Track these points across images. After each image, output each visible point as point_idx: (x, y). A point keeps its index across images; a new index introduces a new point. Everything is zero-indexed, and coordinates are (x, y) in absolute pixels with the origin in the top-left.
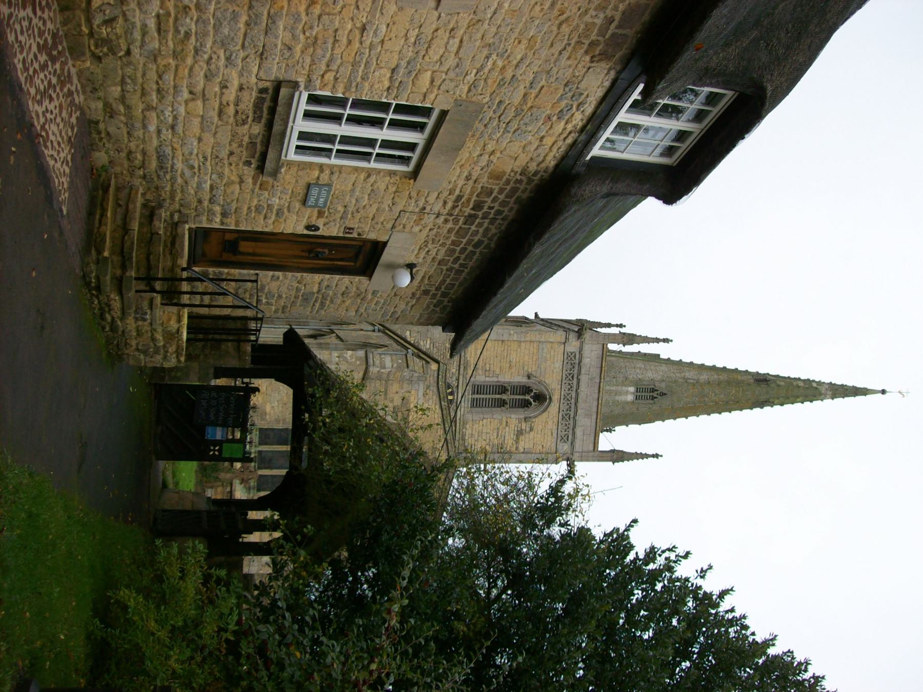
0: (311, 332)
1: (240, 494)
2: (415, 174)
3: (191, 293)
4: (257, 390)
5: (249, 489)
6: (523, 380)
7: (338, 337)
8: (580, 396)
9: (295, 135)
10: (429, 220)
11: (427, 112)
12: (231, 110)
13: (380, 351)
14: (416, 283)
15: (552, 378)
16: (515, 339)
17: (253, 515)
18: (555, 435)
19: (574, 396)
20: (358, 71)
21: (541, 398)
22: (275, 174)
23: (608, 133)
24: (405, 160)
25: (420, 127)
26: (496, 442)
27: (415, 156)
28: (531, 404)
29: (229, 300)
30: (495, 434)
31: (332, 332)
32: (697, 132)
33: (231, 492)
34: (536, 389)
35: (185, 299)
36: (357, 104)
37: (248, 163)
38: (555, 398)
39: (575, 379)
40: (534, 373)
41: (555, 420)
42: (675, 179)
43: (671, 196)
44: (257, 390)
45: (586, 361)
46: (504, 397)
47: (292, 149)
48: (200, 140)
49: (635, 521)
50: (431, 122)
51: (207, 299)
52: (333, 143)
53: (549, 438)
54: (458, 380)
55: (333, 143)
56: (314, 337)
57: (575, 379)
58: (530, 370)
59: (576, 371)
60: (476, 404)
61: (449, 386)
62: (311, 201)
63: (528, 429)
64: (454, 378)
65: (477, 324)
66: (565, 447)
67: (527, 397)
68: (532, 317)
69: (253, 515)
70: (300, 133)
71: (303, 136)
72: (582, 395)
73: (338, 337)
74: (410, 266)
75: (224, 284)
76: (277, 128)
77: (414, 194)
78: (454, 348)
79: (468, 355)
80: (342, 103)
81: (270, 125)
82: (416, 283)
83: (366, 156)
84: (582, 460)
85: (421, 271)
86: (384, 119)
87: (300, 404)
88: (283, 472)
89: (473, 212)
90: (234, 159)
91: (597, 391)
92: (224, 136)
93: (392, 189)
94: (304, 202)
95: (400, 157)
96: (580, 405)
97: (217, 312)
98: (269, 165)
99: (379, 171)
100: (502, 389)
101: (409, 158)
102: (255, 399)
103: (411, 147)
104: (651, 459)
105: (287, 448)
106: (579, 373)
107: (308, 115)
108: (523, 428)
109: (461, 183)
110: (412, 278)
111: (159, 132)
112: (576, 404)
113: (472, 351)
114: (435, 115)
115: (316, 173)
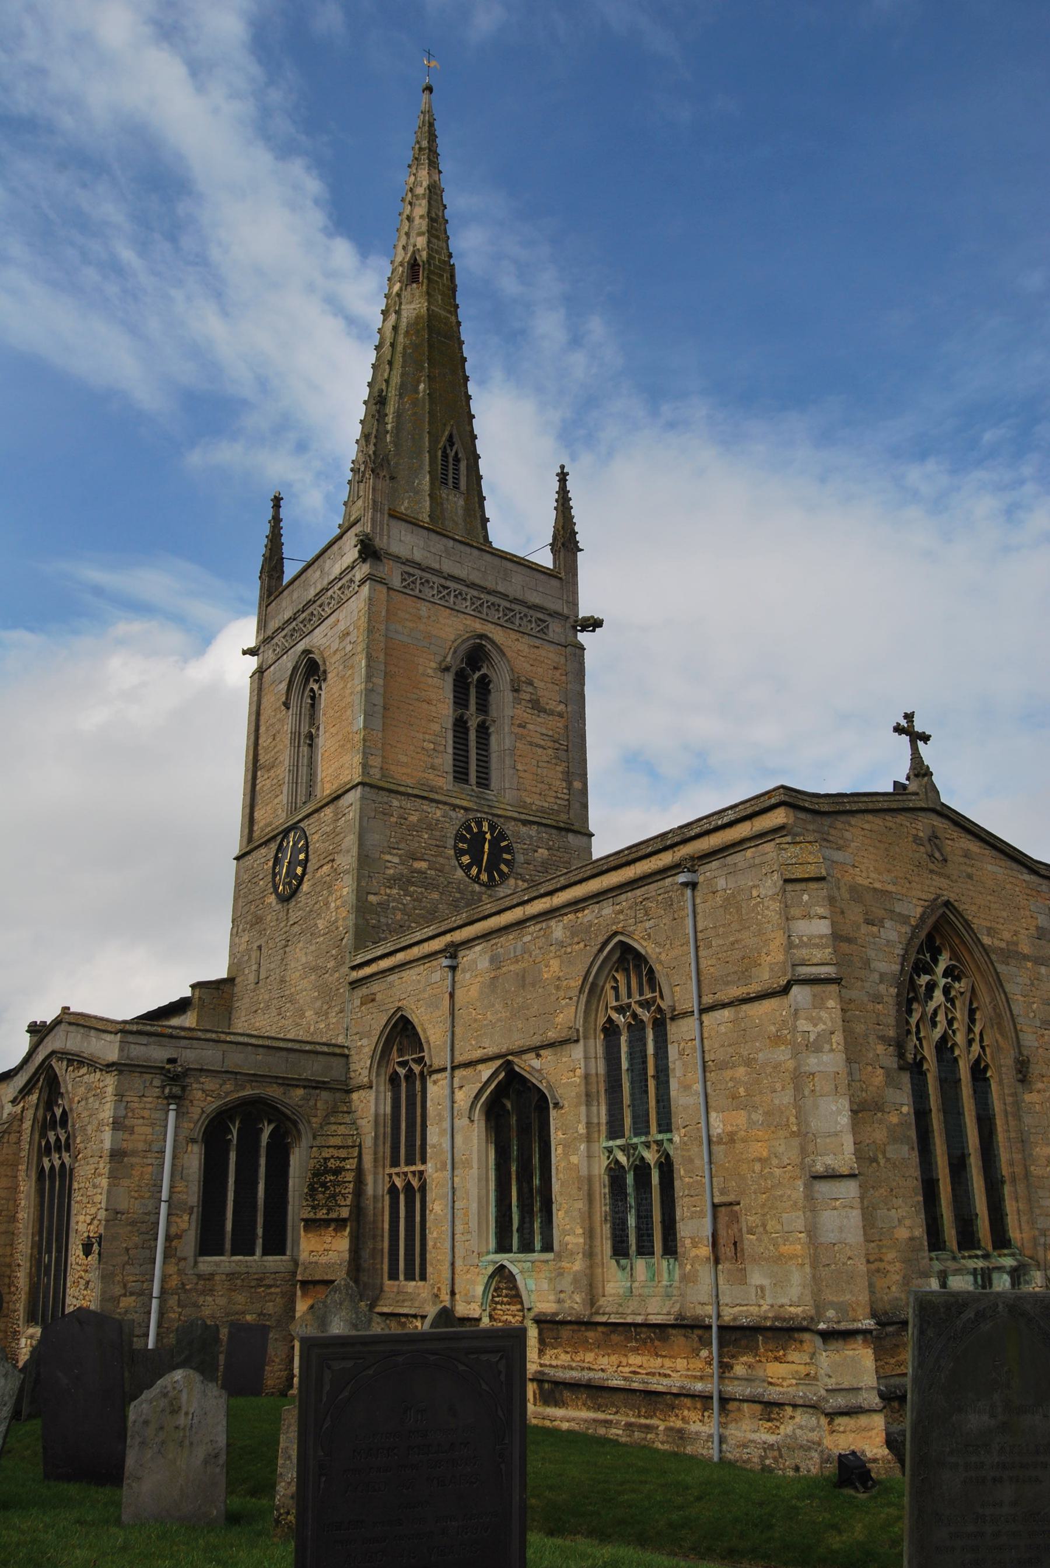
6: (449, 678)
8: (477, 581)
15: (451, 628)
16: (381, 682)
18: (538, 642)
19: (475, 593)
20: (244, 1089)
26: (550, 752)
28: (485, 676)
30: (540, 751)
38: (479, 627)
39: (448, 583)
40: (439, 659)
41: (514, 636)
45: (418, 556)
49: (245, 653)
53: (543, 653)
54: (455, 807)
57: (448, 583)
58: (433, 665)
59: (435, 579)
63: (530, 689)
64: (453, 814)
66: (556, 629)
68: (253, 662)
72: (475, 577)
79: (410, 782)
84: (575, 604)
91: (468, 550)
96: (490, 584)
100: (460, 726)
104: (569, 486)
106: (438, 573)
108: (527, 697)
112: (489, 593)
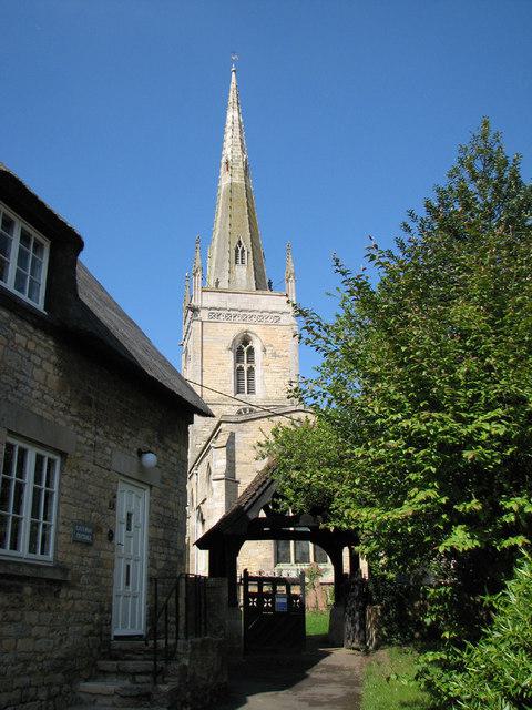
0: (200, 524)
1: (330, 577)
2: (63, 455)
3: (166, 638)
4: (245, 572)
5: (326, 570)
7: (203, 502)
9: (32, 556)
10: (100, 440)
11: (10, 447)
12: (11, 614)
13: (212, 469)
14: (153, 449)
17: (346, 568)
21: (246, 341)
22: (64, 570)
23: (25, 297)
24: (51, 463)
25: (23, 453)
27: (47, 455)
29: (172, 601)
31: (199, 507)
32: (21, 224)
33: (329, 584)
34: (238, 343)
35: (171, 642)
36: (7, 470)
37: (56, 594)
38: (245, 327)
42: (66, 243)
43: (78, 244)
44: (245, 572)
46: (245, 369)
47: (44, 557)
48: (37, 638)
50: (18, 444)
51: (172, 619)
52: (40, 490)
55: (40, 490)
56: (203, 522)
60: (251, 391)
61: (239, 413)
62: (87, 538)
65: (188, 398)
67: (245, 349)
69: (346, 568)
70: (30, 552)
71: (32, 549)
73: (203, 502)
74: (140, 453)
75: (160, 607)
76: (27, 572)
77: (78, 454)
78: (207, 414)
80: (6, 482)
81: (26, 579)
82: (153, 449)
83: (48, 496)
85: (144, 445)
86: (16, 482)
87: (258, 535)
88: (311, 545)
89: (93, 406)
90: (53, 606)
92: (32, 617)
93: (75, 473)
94: (89, 544)
95: (49, 466)
97: (182, 609)
98: (59, 576)
99: (60, 484)
100: (239, 371)
101: (49, 459)
102: (254, 572)
103: (39, 459)
105: (292, 542)
107: (14, 546)
109: (69, 417)
110: (149, 452)
111: (30, 674)
113: (208, 396)
114: (11, 440)
115: (62, 536)
